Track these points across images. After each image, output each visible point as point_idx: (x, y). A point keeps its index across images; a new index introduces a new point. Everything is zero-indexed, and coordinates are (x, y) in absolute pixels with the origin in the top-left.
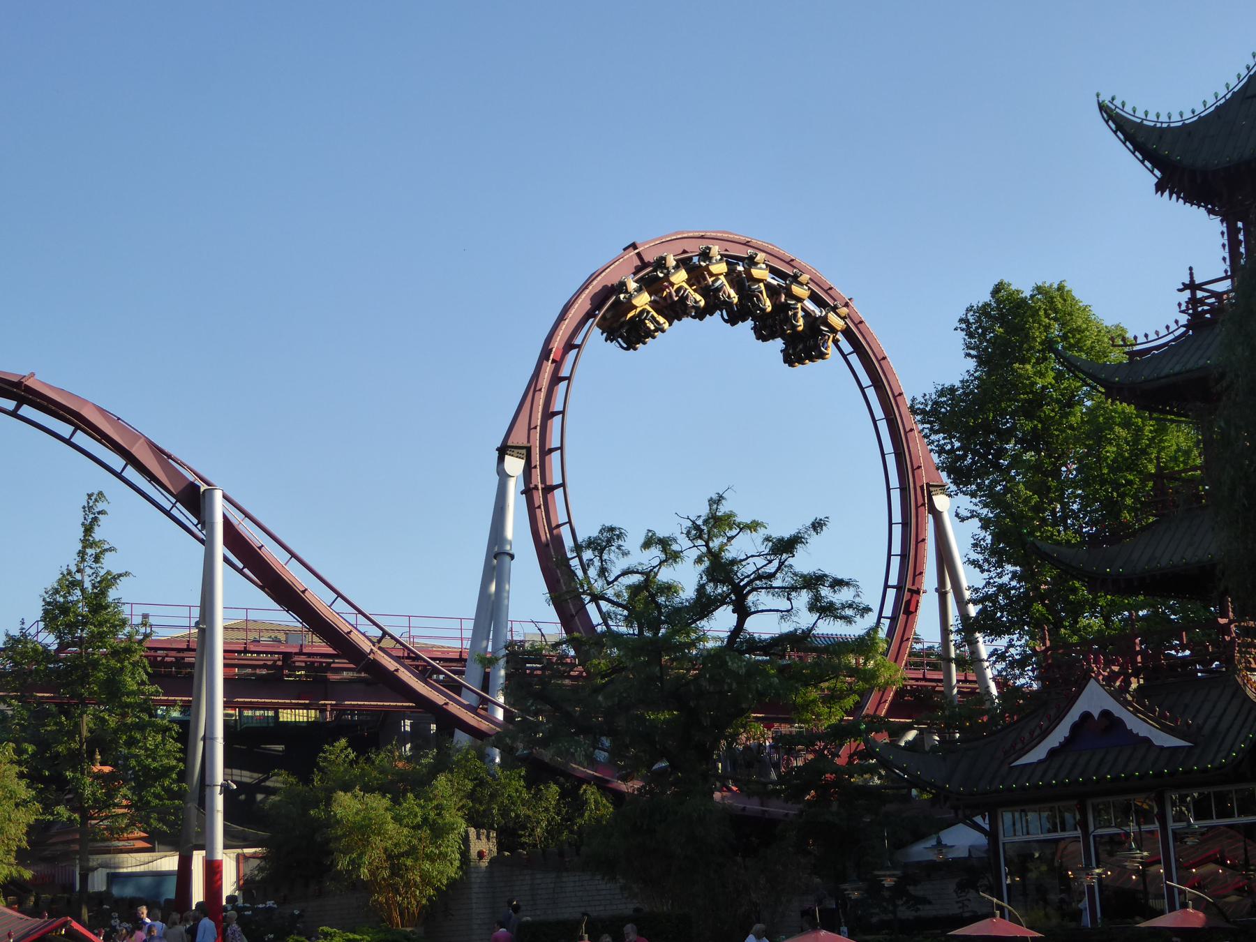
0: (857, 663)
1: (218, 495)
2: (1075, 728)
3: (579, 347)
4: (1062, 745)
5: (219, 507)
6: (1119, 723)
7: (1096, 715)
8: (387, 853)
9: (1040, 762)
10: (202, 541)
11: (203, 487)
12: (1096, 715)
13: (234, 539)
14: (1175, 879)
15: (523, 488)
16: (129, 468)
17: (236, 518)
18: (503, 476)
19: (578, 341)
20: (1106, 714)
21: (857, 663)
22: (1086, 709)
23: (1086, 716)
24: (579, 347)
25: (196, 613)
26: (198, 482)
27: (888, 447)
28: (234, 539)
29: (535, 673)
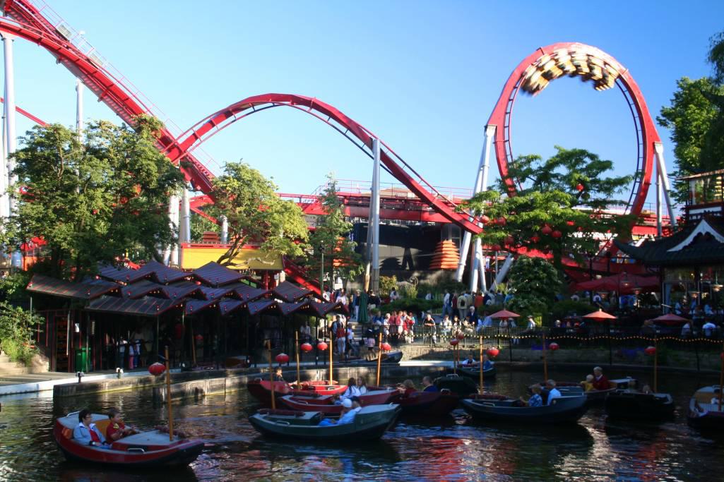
0: (718, 180)
1: (378, 142)
2: (695, 238)
3: (512, 100)
4: (689, 245)
5: (379, 146)
6: (713, 237)
7: (704, 233)
8: (423, 275)
9: (680, 251)
10: (372, 158)
11: (374, 139)
12: (704, 233)
13: (384, 158)
14: (667, 302)
15: (493, 141)
16: (349, 131)
17: (385, 150)
18: (486, 136)
19: (512, 98)
20: (708, 233)
21: (718, 180)
22: (699, 231)
23: (700, 234)
24: (512, 100)
25: (371, 184)
26: (372, 137)
27: (639, 128)
28: (384, 158)
29: (166, 347)
